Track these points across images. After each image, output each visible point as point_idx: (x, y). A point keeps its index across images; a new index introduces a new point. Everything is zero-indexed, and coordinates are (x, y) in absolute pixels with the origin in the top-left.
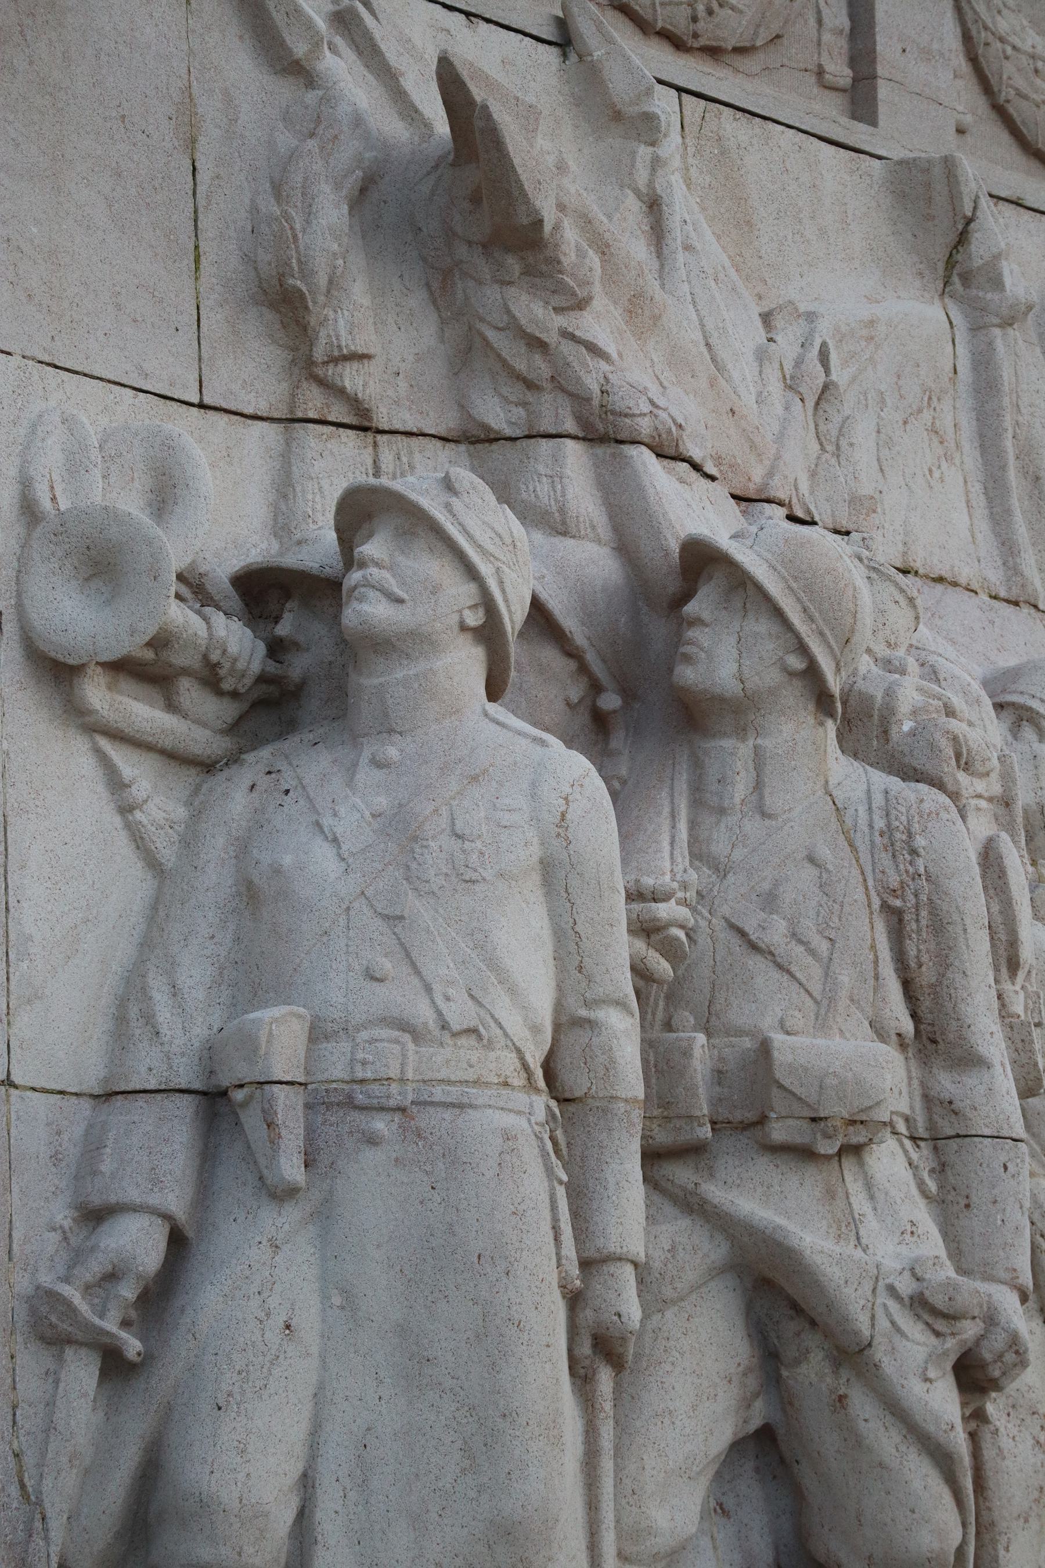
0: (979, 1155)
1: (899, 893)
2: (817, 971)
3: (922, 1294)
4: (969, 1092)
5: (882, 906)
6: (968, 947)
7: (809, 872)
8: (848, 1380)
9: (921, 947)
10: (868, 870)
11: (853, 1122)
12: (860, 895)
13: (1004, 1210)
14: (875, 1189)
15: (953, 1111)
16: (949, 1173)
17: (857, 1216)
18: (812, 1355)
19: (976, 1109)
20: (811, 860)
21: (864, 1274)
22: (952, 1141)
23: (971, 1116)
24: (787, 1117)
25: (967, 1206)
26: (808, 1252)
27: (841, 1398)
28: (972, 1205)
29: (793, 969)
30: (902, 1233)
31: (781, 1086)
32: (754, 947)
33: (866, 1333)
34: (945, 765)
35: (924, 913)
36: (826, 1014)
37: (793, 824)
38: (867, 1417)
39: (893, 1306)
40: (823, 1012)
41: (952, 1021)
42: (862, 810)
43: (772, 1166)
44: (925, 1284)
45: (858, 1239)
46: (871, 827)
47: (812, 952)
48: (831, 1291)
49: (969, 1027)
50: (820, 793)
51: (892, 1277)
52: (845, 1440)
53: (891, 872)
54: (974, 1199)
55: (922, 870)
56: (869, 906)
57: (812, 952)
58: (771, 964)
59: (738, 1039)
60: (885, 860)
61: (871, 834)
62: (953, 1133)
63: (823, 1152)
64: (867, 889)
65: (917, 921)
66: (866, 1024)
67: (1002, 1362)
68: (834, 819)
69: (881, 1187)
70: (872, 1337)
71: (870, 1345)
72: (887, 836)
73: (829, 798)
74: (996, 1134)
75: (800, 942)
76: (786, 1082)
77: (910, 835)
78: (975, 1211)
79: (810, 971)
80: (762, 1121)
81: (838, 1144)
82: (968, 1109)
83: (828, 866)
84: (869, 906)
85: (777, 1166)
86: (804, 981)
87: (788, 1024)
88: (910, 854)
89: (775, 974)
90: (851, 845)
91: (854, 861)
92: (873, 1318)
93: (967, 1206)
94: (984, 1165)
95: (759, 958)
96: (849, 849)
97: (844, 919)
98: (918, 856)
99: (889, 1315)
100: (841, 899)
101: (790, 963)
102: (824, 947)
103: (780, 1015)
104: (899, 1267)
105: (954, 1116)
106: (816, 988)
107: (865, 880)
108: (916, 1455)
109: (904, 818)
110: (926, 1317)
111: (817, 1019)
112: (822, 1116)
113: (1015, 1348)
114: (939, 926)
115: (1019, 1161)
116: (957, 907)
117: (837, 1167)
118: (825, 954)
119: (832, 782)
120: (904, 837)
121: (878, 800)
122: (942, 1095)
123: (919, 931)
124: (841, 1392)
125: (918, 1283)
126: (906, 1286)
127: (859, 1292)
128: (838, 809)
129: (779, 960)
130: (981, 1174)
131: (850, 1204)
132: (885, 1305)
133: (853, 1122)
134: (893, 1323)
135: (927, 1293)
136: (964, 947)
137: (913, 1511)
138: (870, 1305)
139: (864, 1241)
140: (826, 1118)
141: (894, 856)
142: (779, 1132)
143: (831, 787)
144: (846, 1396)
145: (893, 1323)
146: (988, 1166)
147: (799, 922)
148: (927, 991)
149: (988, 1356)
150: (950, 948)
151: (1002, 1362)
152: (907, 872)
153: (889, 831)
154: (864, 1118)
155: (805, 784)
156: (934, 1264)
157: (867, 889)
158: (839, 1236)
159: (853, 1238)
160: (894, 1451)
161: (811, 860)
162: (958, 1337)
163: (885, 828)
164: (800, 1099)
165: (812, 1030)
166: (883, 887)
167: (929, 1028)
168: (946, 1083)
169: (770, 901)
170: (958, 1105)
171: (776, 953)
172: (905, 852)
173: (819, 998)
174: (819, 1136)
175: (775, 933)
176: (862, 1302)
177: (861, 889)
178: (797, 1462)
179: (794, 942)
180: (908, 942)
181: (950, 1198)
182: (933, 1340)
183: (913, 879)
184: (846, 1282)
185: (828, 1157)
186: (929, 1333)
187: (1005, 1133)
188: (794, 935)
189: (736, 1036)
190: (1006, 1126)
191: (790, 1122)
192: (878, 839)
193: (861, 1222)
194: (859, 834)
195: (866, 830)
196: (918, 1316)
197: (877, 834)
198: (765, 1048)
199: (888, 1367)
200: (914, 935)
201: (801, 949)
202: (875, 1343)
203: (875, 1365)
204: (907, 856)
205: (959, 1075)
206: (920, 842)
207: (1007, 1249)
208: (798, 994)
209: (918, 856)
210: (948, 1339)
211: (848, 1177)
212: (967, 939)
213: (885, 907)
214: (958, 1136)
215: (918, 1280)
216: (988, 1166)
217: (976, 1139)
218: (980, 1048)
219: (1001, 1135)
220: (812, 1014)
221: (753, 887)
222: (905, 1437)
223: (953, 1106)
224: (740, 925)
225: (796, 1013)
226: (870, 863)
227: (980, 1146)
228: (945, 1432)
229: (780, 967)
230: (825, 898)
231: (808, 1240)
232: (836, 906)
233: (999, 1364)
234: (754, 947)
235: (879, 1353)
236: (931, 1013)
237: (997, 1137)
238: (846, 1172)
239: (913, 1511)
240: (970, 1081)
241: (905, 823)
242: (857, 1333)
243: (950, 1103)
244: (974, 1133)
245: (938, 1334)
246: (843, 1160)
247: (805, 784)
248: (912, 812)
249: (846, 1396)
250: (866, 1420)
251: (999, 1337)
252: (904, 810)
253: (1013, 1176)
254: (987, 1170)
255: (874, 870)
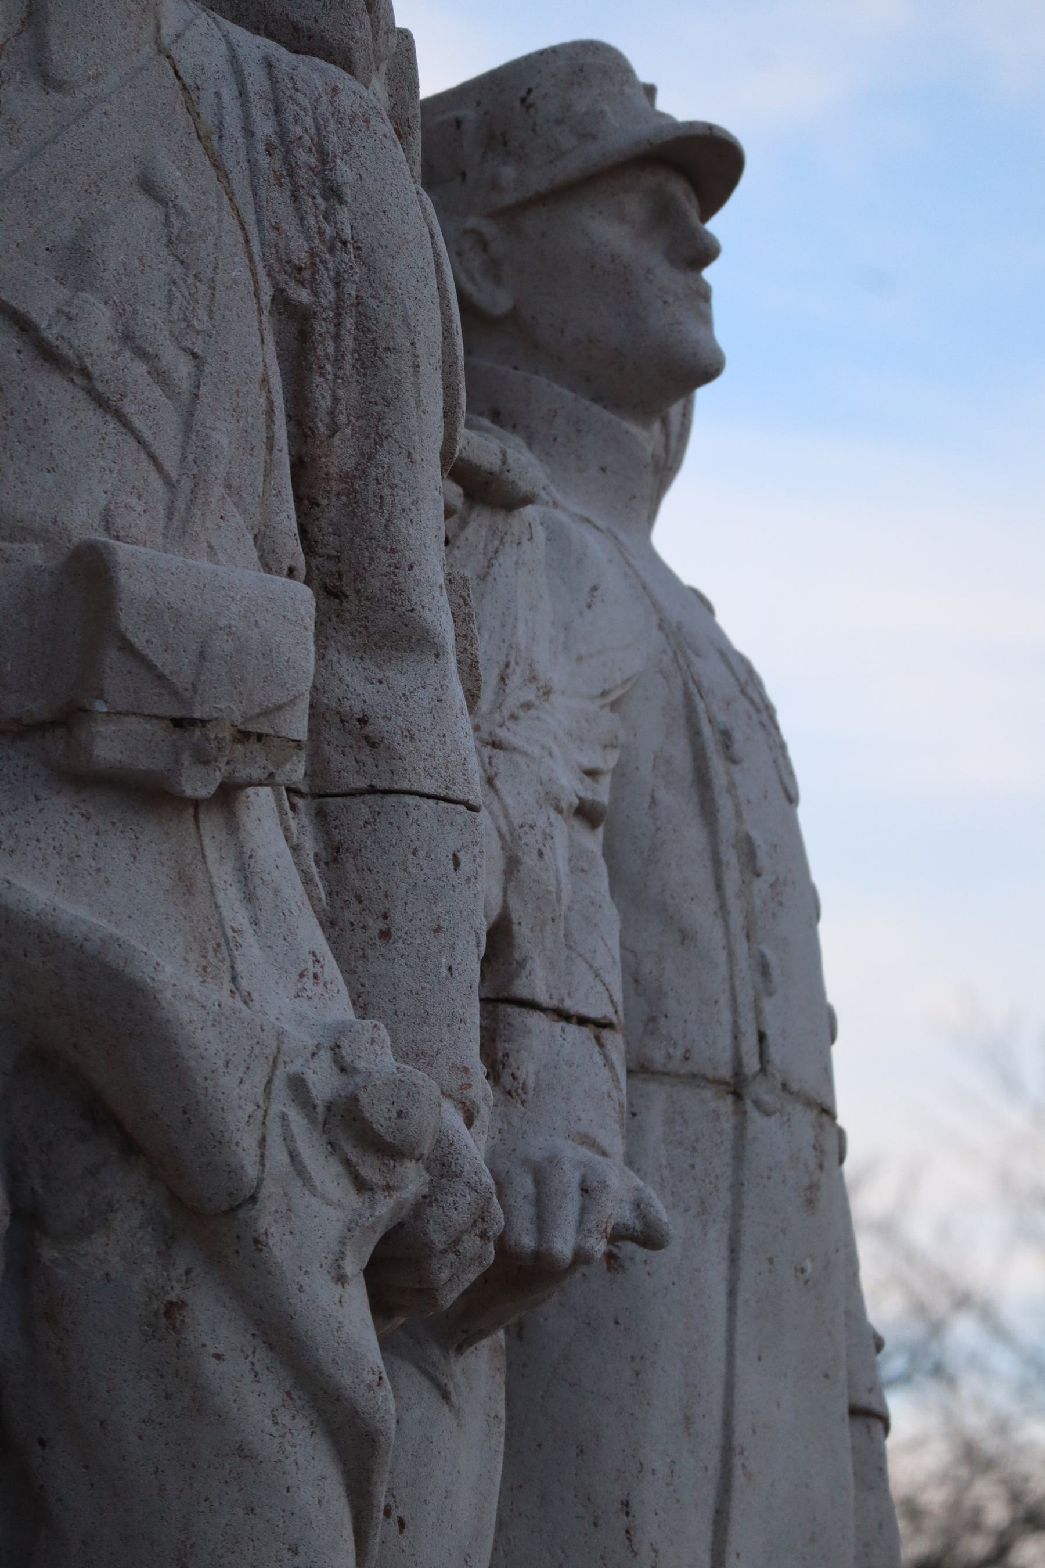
0: (412, 831)
1: (307, 274)
2: (170, 418)
3: (355, 1099)
4: (402, 702)
5: (273, 299)
6: (418, 402)
7: (144, 212)
8: (188, 1272)
9: (341, 393)
10: (250, 218)
11: (243, 736)
12: (240, 271)
13: (453, 947)
14: (257, 881)
15: (367, 738)
16: (350, 866)
17: (230, 933)
18: (120, 1215)
19: (412, 739)
20: (148, 186)
21: (257, 1049)
22: (358, 800)
23: (404, 752)
24: (127, 714)
25: (385, 935)
26: (168, 994)
27: (173, 1309)
28: (395, 934)
29: (129, 408)
30: (301, 976)
31: (127, 647)
32: (48, 355)
33: (252, 1171)
34: (356, 24)
35: (349, 323)
36: (188, 509)
37: (107, 107)
38: (221, 1350)
39: (297, 1120)
40: (181, 504)
41: (380, 553)
42: (229, 93)
43: (77, 817)
44: (358, 1079)
45: (234, 979)
46: (249, 132)
47: (161, 377)
48: (200, 1080)
49: (411, 568)
50: (148, 49)
51: (300, 1061)
52: (168, 1397)
53: (291, 228)
54: (398, 918)
55: (347, 233)
56: (256, 295)
57: (161, 377)
58: (81, 395)
59: (16, 546)
60: (279, 202)
61: (250, 149)
62: (361, 784)
63: (189, 792)
64: (251, 260)
65: (337, 337)
66: (250, 537)
67: (457, 1253)
68: (180, 108)
69: (267, 878)
70: (260, 1181)
71: (253, 1199)
72: (278, 154)
73: (167, 63)
74: (443, 793)
75: (141, 353)
76: (138, 640)
77: (324, 158)
78: (400, 945)
79: (158, 417)
80: (70, 718)
81: (218, 777)
82: (398, 737)
83: (180, 202)
84: (256, 295)
85: (87, 817)
86: (147, 434)
87: (119, 522)
88: (326, 199)
89: (92, 417)
90: (217, 165)
91: (225, 199)
92: (263, 1142)
93: (385, 935)
94: (421, 854)
95: (57, 380)
96: (212, 173)
97: (217, 317)
98: (341, 201)
99: (288, 1138)
100: (209, 275)
101: (123, 396)
102: (182, 369)
103: (103, 502)
104: (311, 1043)
105: (367, 749)
106: (168, 451)
107: (247, 241)
108: (306, 1433)
109: (309, 121)
110: (348, 1148)
111: (170, 517)
112: (197, 715)
113: (481, 1226)
114: (371, 355)
115: (477, 850)
116: (405, 318)
117: (191, 824)
118: (185, 385)
119: (168, 31)
120: (313, 161)
121: (257, 80)
122: (347, 704)
123: (338, 359)
124: (172, 1296)
125: (343, 1077)
126: (323, 1082)
127: (245, 1087)
128: (184, 87)
129: (100, 387)
130: (414, 870)
131: (217, 907)
132: (284, 1117)
133: (243, 736)
134: (294, 1156)
135: (364, 1098)
136: (413, 403)
137: (295, 1552)
138: (260, 1113)
139: (244, 983)
140: (204, 722)
141: (295, 197)
142: (110, 745)
143: (166, 41)
144: (181, 1305)
145: (294, 1156)
146: (428, 855)
147: (135, 312)
148: (336, 486)
149: (439, 1239)
150: (388, 403)
151: (457, 1253)
152: (321, 233)
153: (283, 144)
154: (265, 729)
155: (124, 27)
156: (373, 1041)
157: (251, 260)
158: (204, 968)
159: (227, 977)
160: (268, 1422)
161: (148, 186)
162: (396, 1195)
163: (274, 139)
164: (160, 677)
165: (160, 540)
166: (279, 260)
167: (329, 565)
168: (358, 684)
169: (76, 261)
170: (378, 726)
171: (95, 372)
172: (316, 192)
173: (174, 474)
174: (186, 758)
175: (95, 334)
176: (250, 1108)
177: (241, 258)
178: (42, 1443)
179: (128, 354)
180: (319, 380)
181: (348, 916)
182: (352, 1199)
183: (331, 250)
184: (227, 1064)
185: (196, 804)
186: (346, 1183)
187: (457, 793)
188: (127, 337)
189: (12, 539)
190: (459, 778)
191: (133, 724)
192: (264, 160)
193: (238, 946)
194: (227, 144)
195: (239, 135)
196: (333, 1145)
197: (261, 148)
198: (90, 571)
199: (280, 1247)
200: (329, 367)
201: (139, 369)
202: (264, 1192)
203: (256, 1241)
204: (319, 200)
205: (379, 667)
206: (344, 172)
207: (455, 1027)
208: (136, 461)
209: (341, 201)
210: (380, 1196)
211: (212, 855)
212: (417, 387)
213: (282, 302)
214: (372, 790)
215: (343, 1070)
216: (428, 855)
217: (408, 799)
218: (426, 614)
219: (452, 795)
220: (160, 507)
221: (38, 231)
222: (289, 1394)
223: (368, 729)
224: (22, 308)
225: (133, 501)
226: (251, 207)
227: (415, 814)
228: (370, 1388)
229: (101, 402)
230: (179, 269)
231: (169, 969)
232: (203, 288)
233: (451, 1257)
234: (48, 355)
235: (266, 1218)
236: (336, 533)
237: (445, 799)
238: (206, 841)
239: (295, 1552)
240: (403, 681)
241: (313, 131)
242: (234, 1172)
243: (363, 721)
244: (405, 785)
245: (361, 1185)
246: (202, 816)
247: (124, 27)
248: (321, 109)
249: (181, 1305)
250: (218, 1357)
251: (461, 1202)
252: (306, 103)
253: (469, 879)
254: (425, 864)
255: (259, 222)
